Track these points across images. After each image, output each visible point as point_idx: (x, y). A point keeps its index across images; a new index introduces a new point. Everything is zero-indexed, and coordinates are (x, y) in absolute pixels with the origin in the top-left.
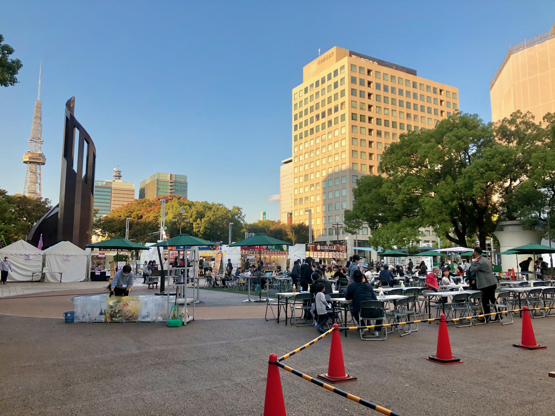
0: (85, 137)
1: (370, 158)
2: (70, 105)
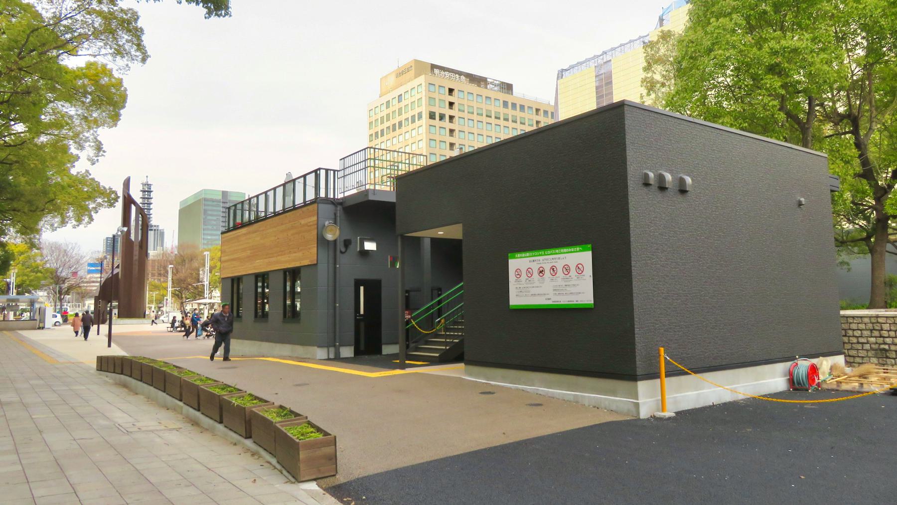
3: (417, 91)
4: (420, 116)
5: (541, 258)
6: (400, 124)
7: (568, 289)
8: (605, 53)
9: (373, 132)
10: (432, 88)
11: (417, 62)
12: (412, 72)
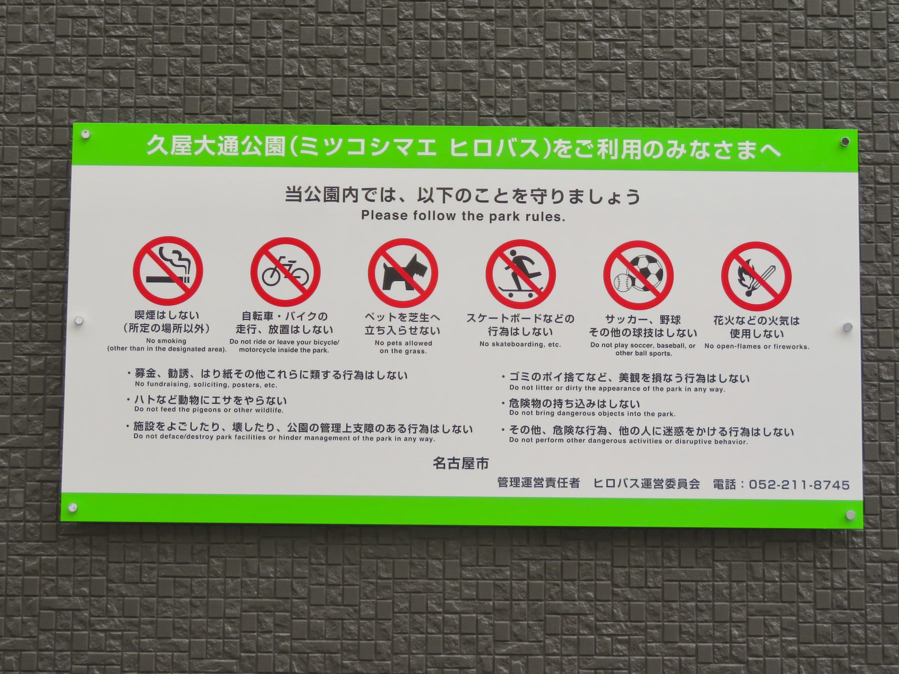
5: (406, 182)
7: (649, 399)
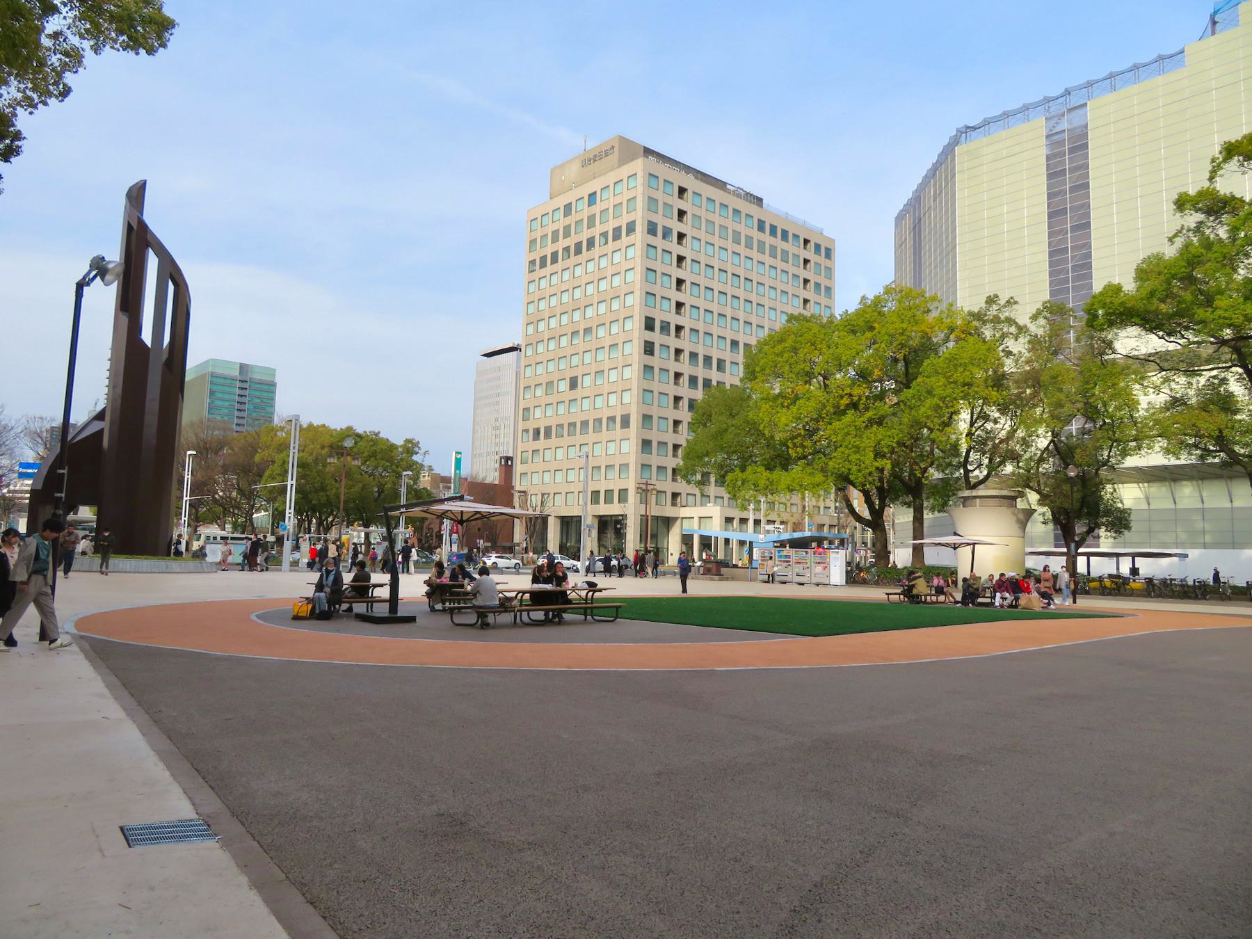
0: (171, 273)
1: (676, 382)
2: (137, 195)
3: (627, 189)
4: (631, 228)
6: (591, 243)
8: (1068, 92)
9: (536, 256)
10: (653, 182)
11: (624, 141)
12: (615, 157)
